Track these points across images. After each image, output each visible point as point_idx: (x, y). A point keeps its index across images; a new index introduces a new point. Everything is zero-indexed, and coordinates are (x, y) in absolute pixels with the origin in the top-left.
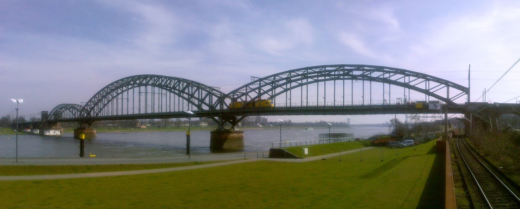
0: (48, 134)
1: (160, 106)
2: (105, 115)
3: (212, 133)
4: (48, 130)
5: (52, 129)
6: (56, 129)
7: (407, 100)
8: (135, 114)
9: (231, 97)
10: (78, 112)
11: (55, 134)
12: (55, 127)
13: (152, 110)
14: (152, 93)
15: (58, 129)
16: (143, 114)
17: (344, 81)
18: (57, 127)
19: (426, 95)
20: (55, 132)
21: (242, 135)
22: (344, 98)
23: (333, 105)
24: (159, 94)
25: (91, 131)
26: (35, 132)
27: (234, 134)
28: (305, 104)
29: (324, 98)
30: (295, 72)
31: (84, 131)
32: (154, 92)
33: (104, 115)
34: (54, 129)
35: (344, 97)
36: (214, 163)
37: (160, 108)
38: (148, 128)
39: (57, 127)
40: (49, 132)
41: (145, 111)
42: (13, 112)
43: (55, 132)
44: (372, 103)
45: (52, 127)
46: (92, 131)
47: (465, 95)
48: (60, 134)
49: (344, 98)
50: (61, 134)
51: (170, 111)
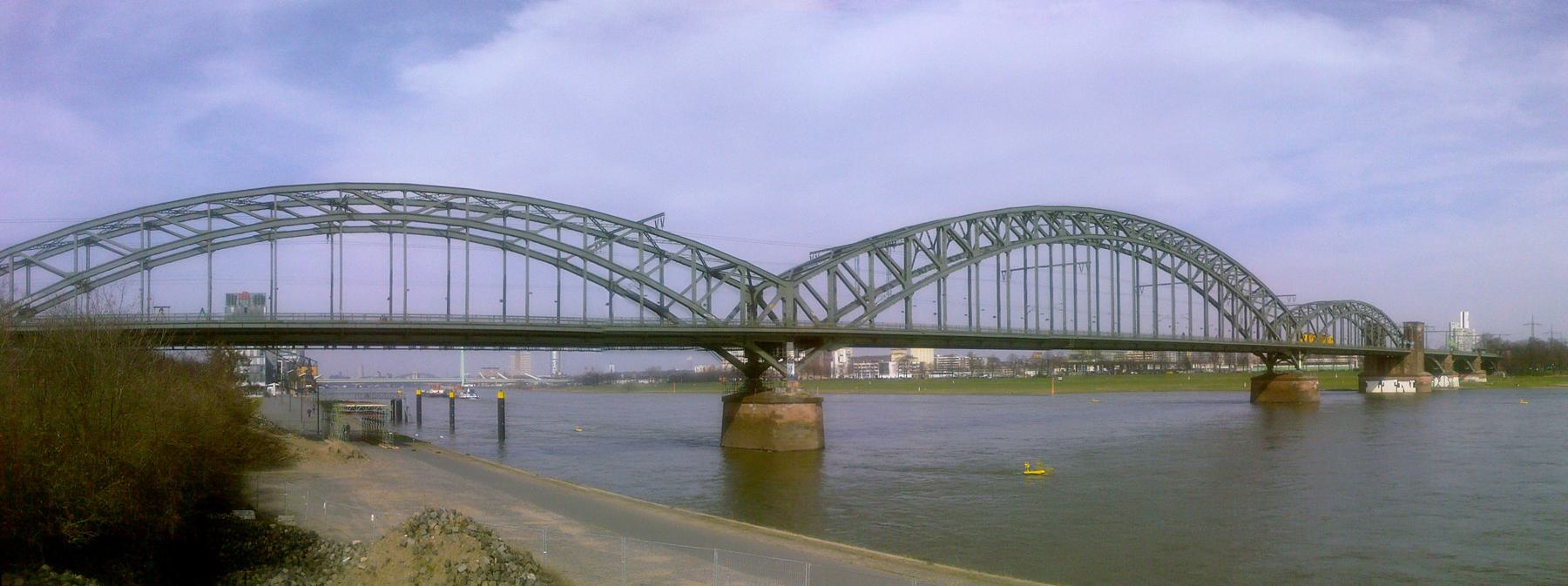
0: (1377, 390)
1: (1094, 314)
2: (1161, 332)
3: (724, 399)
6: (1402, 376)
7: (336, 310)
11: (1400, 390)
12: (1399, 371)
13: (1113, 328)
15: (1407, 376)
17: (449, 242)
20: (1398, 386)
21: (773, 412)
22: (611, 308)
24: (1025, 269)
25: (1294, 382)
27: (751, 405)
28: (458, 310)
29: (607, 304)
31: (1273, 382)
34: (1393, 376)
37: (1116, 326)
38: (651, 386)
39: (1406, 370)
40: (1381, 383)
41: (1134, 329)
42: (1533, 324)
48: (1413, 390)
49: (611, 308)
50: (1417, 390)
51: (1038, 327)
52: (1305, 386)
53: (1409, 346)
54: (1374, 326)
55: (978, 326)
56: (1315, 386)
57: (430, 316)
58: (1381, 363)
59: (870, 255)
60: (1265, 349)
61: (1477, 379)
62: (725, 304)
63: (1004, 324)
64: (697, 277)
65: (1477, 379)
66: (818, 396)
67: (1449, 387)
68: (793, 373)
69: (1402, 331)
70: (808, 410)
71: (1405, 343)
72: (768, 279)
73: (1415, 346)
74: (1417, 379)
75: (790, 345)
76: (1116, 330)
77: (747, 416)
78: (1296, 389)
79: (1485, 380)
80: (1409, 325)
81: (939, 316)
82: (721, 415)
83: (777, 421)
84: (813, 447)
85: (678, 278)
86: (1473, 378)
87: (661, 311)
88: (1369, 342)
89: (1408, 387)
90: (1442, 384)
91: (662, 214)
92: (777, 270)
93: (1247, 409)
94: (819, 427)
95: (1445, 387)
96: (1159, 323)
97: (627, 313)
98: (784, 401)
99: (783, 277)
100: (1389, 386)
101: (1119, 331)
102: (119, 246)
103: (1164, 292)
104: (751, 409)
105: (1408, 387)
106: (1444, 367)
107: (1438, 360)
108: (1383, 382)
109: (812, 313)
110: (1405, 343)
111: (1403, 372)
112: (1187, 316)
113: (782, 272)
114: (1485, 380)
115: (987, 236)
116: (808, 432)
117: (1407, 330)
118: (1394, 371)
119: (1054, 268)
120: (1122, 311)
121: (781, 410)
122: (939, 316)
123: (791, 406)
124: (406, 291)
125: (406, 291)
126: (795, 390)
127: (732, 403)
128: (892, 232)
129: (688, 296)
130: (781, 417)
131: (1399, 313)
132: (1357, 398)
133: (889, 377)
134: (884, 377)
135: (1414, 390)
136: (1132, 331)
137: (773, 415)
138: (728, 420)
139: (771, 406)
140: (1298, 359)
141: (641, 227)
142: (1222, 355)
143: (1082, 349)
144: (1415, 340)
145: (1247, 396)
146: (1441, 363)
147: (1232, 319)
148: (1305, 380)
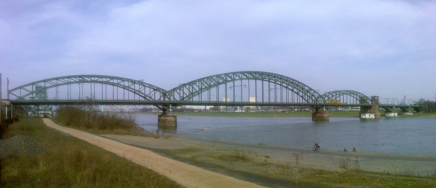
0: (364, 117)
1: (209, 97)
2: (357, 103)
3: (158, 116)
4: (364, 113)
5: (367, 113)
8: (258, 103)
9: (179, 92)
10: (307, 99)
11: (370, 117)
14: (275, 89)
15: (372, 113)
16: (214, 102)
18: (371, 111)
19: (18, 97)
20: (370, 116)
21: (166, 119)
23: (102, 99)
24: (275, 89)
26: (387, 115)
30: (74, 81)
32: (281, 89)
33: (299, 102)
34: (368, 113)
35: (124, 96)
36: (134, 145)
39: (372, 111)
40: (365, 115)
43: (370, 116)
44: (388, 104)
45: (368, 111)
46: (323, 115)
47: (139, 99)
50: (375, 117)
52: (325, 115)
53: (373, 103)
54: (363, 99)
55: (276, 102)
56: (328, 116)
57: (266, 102)
58: (366, 109)
59: (189, 86)
60: (161, 104)
61: (409, 114)
62: (158, 96)
63: (69, 98)
64: (179, 92)
65: (409, 114)
66: (175, 115)
67: (394, 116)
68: (171, 111)
69: (371, 99)
70: (173, 119)
71: (372, 103)
72: (167, 92)
73: (374, 103)
74: (375, 114)
75: (170, 105)
76: (218, 101)
77: (162, 119)
78: (322, 116)
79: (412, 114)
80: (373, 97)
81: (292, 100)
82: (158, 119)
83: (167, 120)
84: (174, 126)
85: (147, 91)
86: (408, 113)
87: (145, 98)
88: (361, 103)
89: (372, 116)
90: (392, 115)
91: (143, 80)
92: (168, 90)
93: (311, 121)
94: (176, 122)
95: (392, 116)
96: (262, 98)
97: (137, 98)
98: (168, 116)
99: (169, 91)
100: (367, 116)
101: (218, 101)
102: (25, 89)
103: (278, 91)
104: (163, 118)
105: (372, 116)
106: (408, 110)
107: (406, 108)
108: (366, 114)
109: (177, 98)
110: (372, 103)
111: (371, 112)
112: (241, 96)
113: (169, 90)
114: (412, 114)
115: (222, 80)
116: (173, 123)
117: (372, 98)
118: (369, 111)
119: (235, 87)
120: (219, 95)
121: (167, 118)
122: (292, 100)
123: (169, 117)
124: (70, 95)
125: (70, 95)
126: (171, 114)
127: (160, 116)
128: (196, 80)
129: (149, 95)
130: (168, 120)
131: (369, 94)
132: (358, 119)
133: (238, 111)
134: (236, 111)
135: (374, 117)
136: (225, 101)
137: (166, 119)
138: (159, 120)
139: (166, 117)
140: (324, 108)
141: (139, 81)
142: (350, 107)
143: (268, 106)
144: (375, 102)
145: (311, 118)
146: (391, 109)
147: (302, 97)
148: (325, 114)
